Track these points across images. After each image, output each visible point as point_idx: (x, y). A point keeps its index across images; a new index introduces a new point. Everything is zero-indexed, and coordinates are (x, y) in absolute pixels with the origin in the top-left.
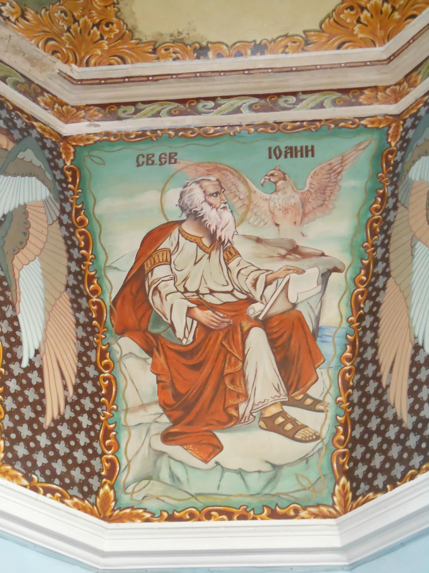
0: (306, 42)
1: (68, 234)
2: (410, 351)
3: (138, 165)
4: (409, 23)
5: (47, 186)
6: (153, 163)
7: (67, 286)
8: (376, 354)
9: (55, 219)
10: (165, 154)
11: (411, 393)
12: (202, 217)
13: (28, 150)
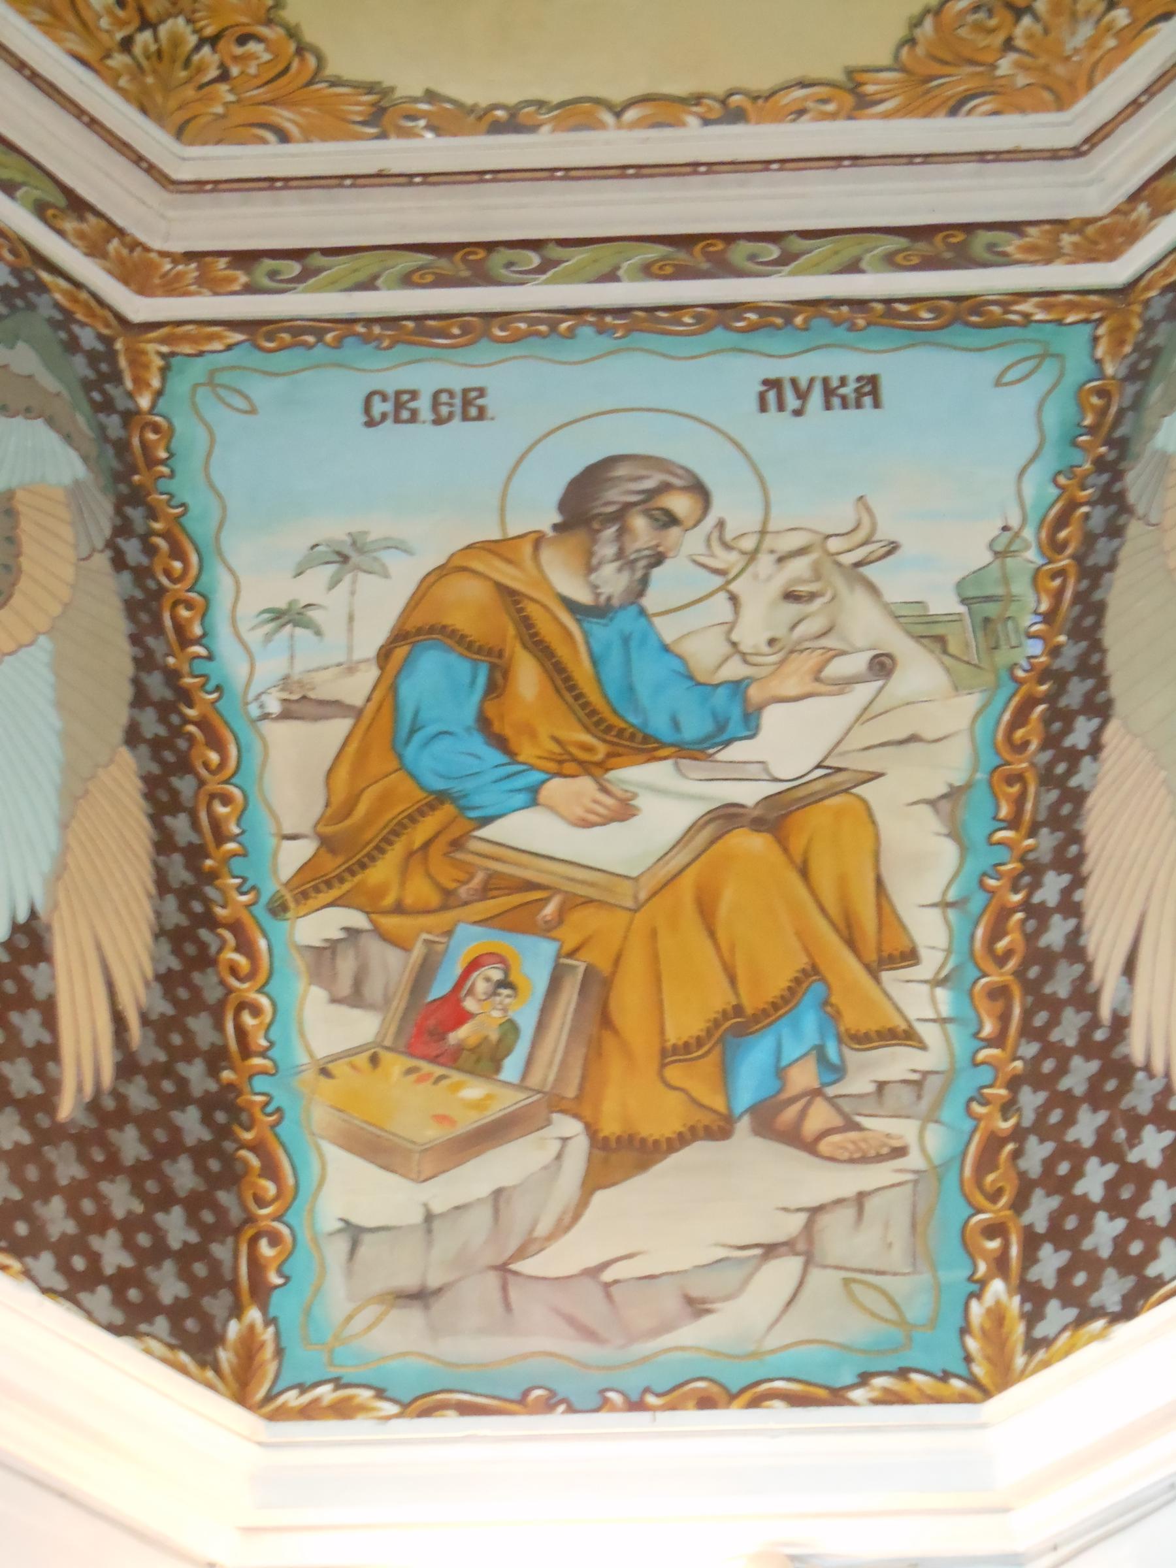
3: (371, 423)
6: (414, 417)
8: (1077, 932)
10: (451, 394)
13: (21, 346)
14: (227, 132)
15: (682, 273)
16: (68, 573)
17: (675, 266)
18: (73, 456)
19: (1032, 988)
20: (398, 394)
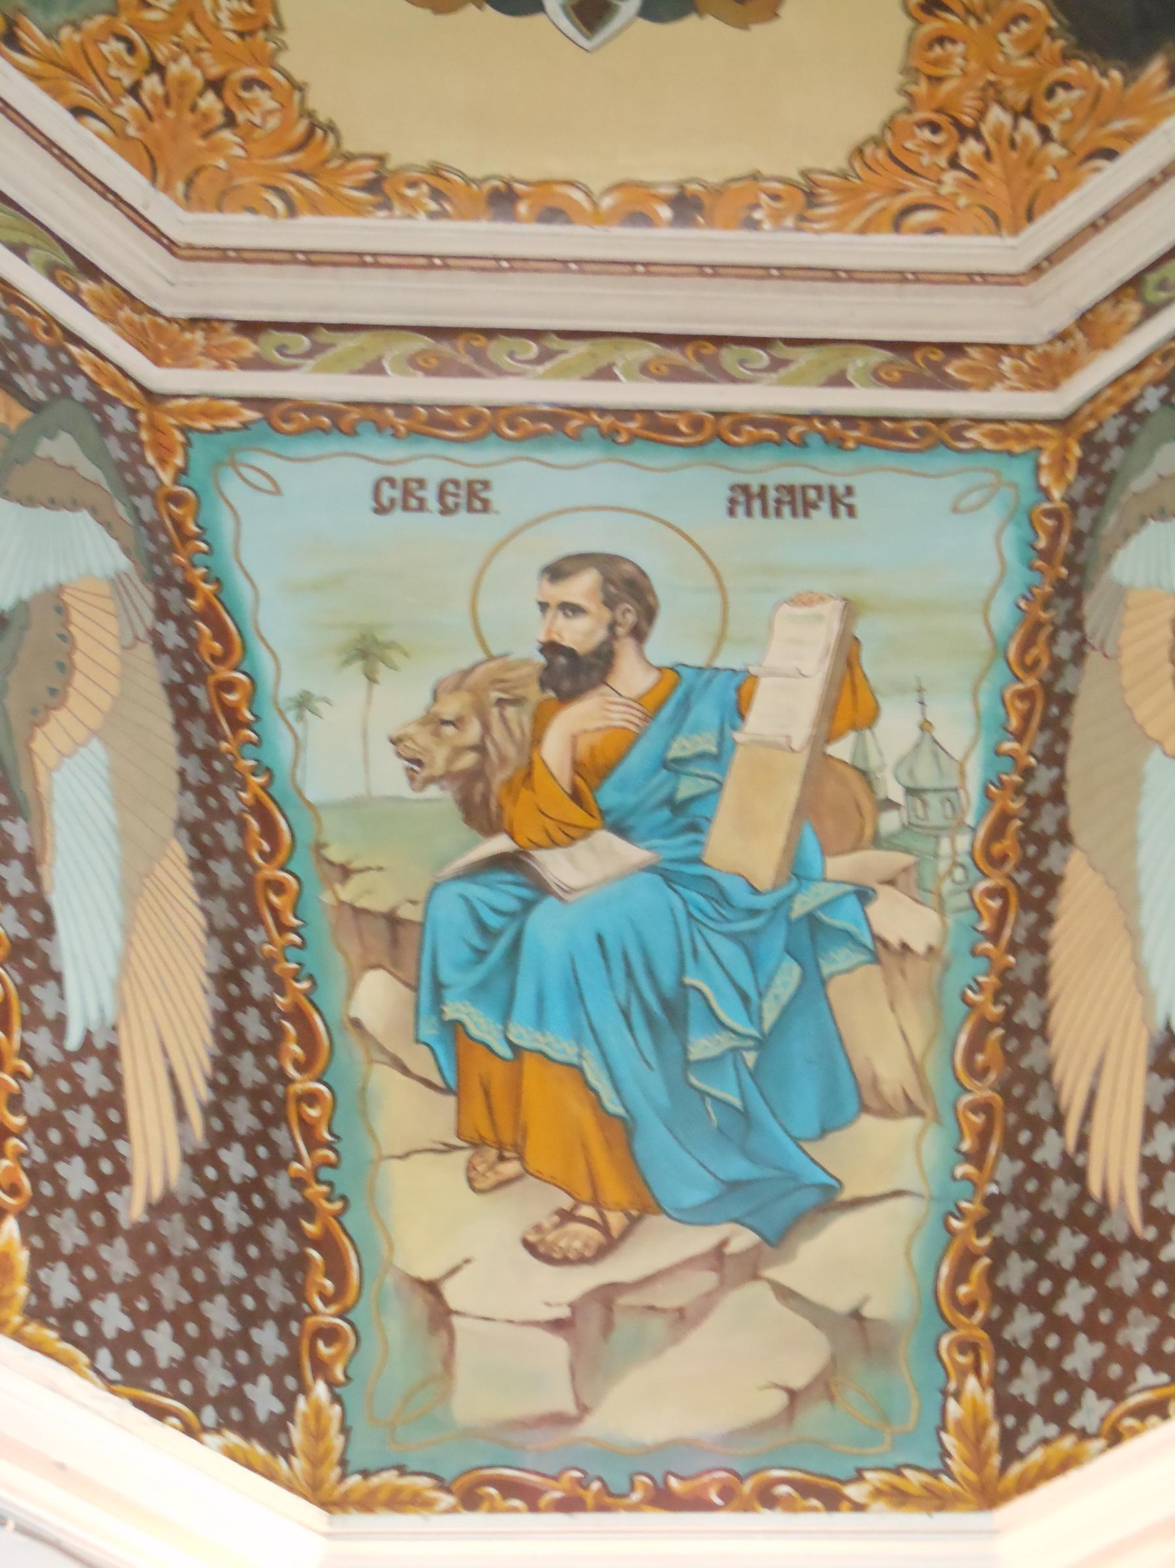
0: (806, 197)
1: (177, 678)
4: (1097, 170)
5: (116, 539)
6: (422, 506)
7: (181, 823)
9: (142, 633)
10: (456, 483)
14: (223, 199)
15: (679, 374)
16: (112, 663)
18: (114, 544)
19: (1016, 1105)
20: (406, 481)
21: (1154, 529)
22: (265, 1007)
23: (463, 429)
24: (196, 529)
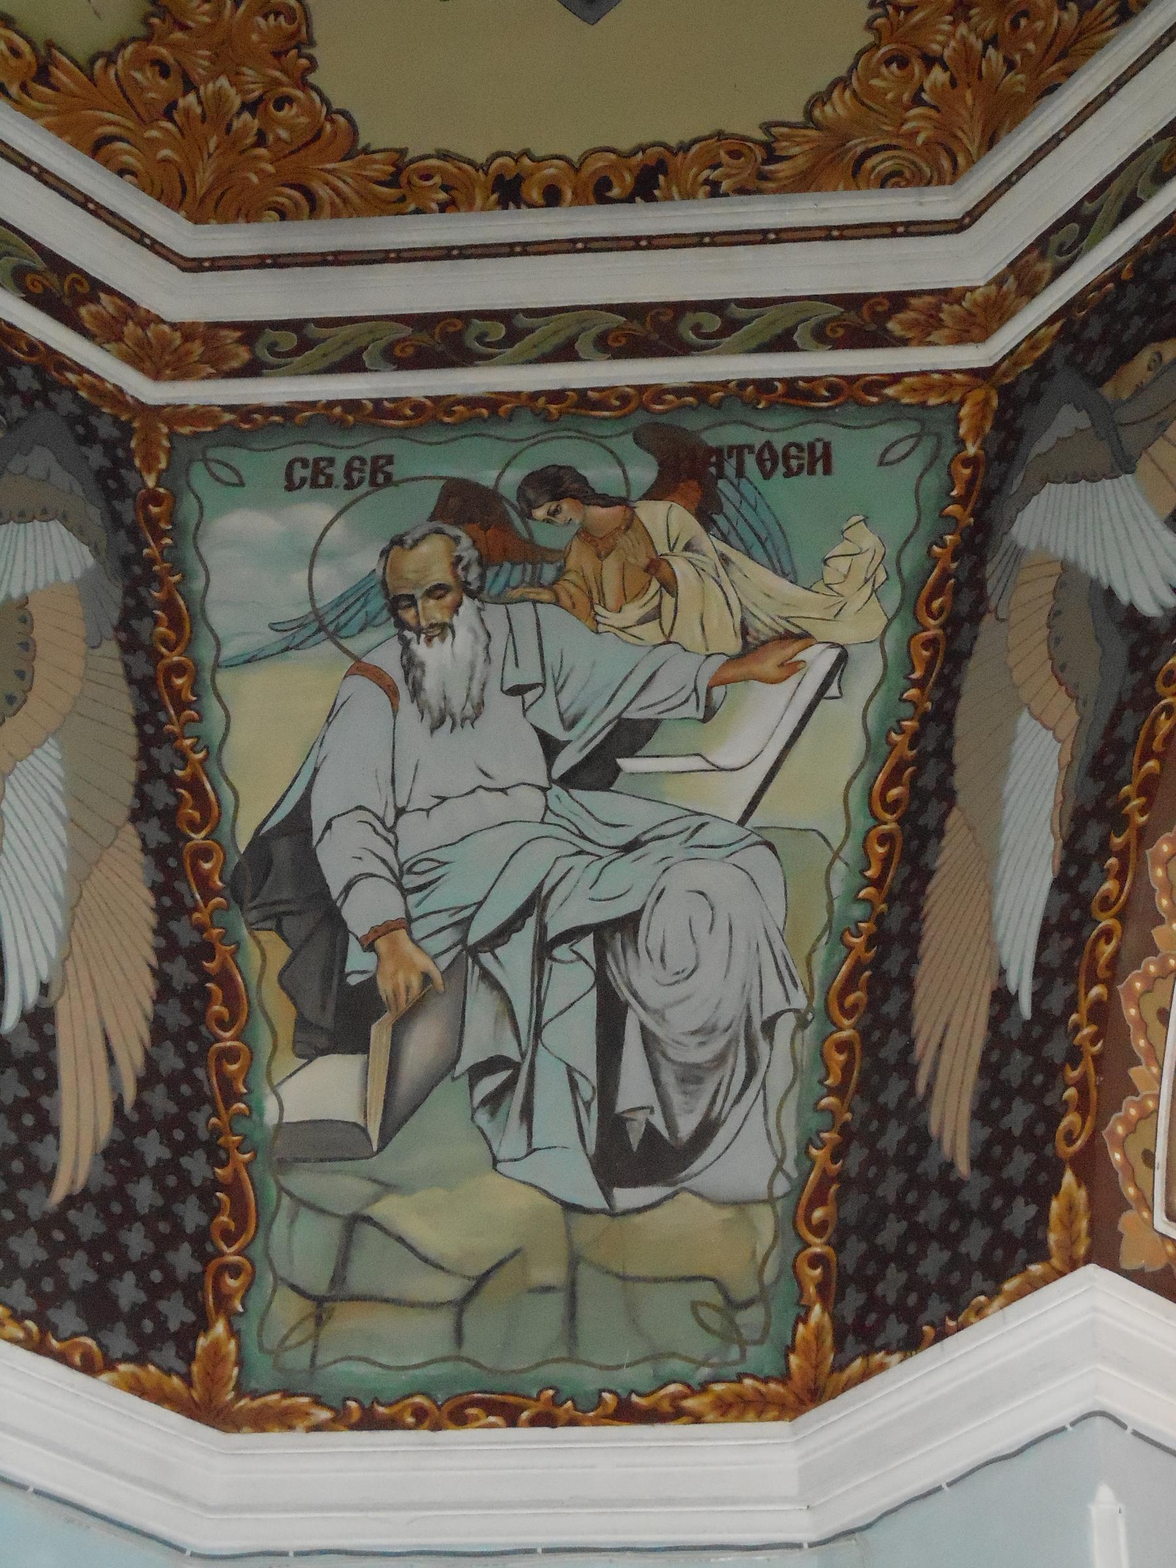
2: (982, 1010)
10: (363, 461)
11: (982, 1113)
12: (429, 640)
17: (416, 347)
21: (1050, 488)
22: (172, 782)
23: (406, 418)
24: (245, 1091)
